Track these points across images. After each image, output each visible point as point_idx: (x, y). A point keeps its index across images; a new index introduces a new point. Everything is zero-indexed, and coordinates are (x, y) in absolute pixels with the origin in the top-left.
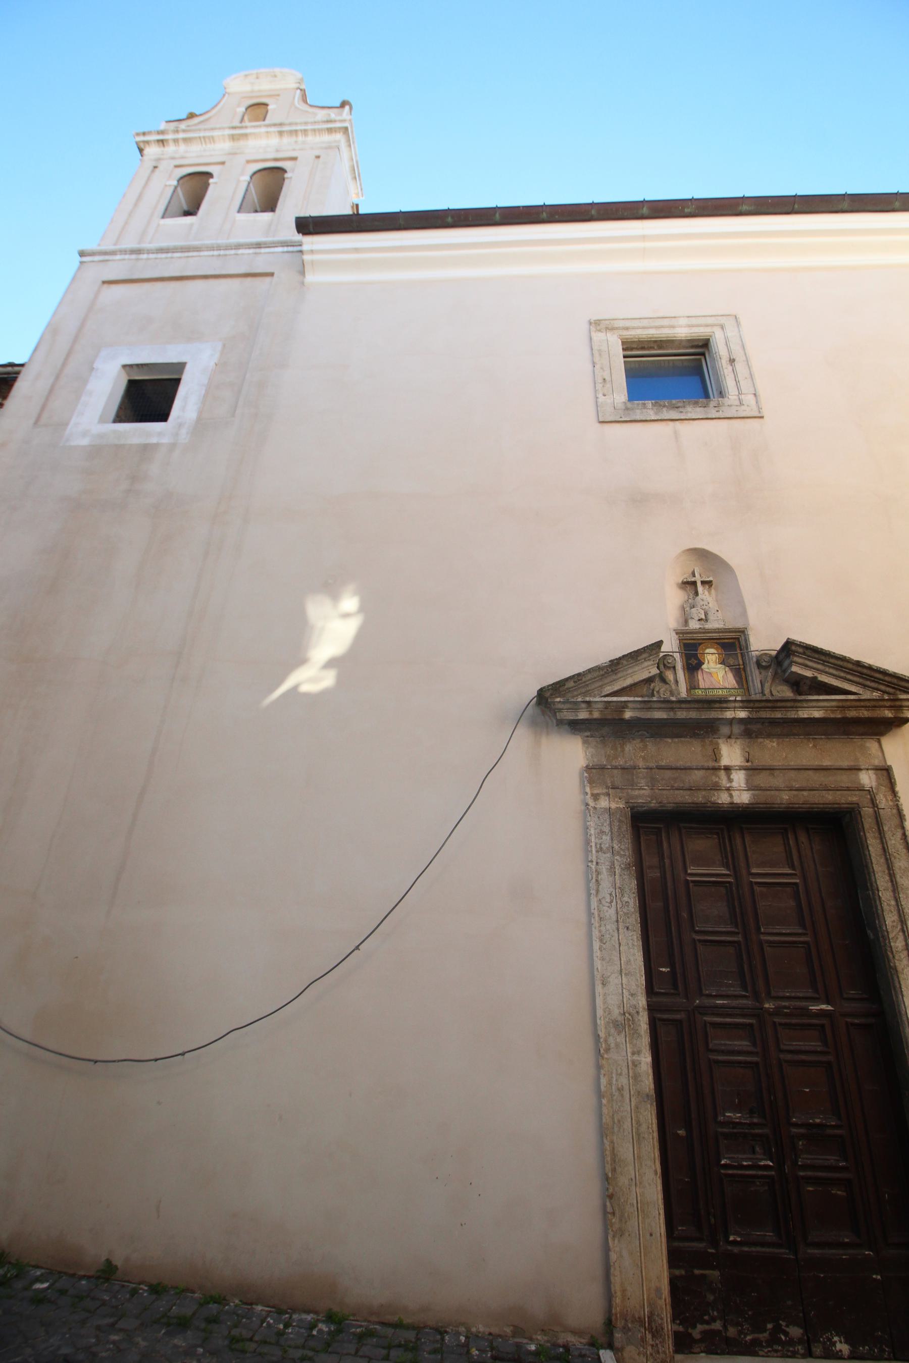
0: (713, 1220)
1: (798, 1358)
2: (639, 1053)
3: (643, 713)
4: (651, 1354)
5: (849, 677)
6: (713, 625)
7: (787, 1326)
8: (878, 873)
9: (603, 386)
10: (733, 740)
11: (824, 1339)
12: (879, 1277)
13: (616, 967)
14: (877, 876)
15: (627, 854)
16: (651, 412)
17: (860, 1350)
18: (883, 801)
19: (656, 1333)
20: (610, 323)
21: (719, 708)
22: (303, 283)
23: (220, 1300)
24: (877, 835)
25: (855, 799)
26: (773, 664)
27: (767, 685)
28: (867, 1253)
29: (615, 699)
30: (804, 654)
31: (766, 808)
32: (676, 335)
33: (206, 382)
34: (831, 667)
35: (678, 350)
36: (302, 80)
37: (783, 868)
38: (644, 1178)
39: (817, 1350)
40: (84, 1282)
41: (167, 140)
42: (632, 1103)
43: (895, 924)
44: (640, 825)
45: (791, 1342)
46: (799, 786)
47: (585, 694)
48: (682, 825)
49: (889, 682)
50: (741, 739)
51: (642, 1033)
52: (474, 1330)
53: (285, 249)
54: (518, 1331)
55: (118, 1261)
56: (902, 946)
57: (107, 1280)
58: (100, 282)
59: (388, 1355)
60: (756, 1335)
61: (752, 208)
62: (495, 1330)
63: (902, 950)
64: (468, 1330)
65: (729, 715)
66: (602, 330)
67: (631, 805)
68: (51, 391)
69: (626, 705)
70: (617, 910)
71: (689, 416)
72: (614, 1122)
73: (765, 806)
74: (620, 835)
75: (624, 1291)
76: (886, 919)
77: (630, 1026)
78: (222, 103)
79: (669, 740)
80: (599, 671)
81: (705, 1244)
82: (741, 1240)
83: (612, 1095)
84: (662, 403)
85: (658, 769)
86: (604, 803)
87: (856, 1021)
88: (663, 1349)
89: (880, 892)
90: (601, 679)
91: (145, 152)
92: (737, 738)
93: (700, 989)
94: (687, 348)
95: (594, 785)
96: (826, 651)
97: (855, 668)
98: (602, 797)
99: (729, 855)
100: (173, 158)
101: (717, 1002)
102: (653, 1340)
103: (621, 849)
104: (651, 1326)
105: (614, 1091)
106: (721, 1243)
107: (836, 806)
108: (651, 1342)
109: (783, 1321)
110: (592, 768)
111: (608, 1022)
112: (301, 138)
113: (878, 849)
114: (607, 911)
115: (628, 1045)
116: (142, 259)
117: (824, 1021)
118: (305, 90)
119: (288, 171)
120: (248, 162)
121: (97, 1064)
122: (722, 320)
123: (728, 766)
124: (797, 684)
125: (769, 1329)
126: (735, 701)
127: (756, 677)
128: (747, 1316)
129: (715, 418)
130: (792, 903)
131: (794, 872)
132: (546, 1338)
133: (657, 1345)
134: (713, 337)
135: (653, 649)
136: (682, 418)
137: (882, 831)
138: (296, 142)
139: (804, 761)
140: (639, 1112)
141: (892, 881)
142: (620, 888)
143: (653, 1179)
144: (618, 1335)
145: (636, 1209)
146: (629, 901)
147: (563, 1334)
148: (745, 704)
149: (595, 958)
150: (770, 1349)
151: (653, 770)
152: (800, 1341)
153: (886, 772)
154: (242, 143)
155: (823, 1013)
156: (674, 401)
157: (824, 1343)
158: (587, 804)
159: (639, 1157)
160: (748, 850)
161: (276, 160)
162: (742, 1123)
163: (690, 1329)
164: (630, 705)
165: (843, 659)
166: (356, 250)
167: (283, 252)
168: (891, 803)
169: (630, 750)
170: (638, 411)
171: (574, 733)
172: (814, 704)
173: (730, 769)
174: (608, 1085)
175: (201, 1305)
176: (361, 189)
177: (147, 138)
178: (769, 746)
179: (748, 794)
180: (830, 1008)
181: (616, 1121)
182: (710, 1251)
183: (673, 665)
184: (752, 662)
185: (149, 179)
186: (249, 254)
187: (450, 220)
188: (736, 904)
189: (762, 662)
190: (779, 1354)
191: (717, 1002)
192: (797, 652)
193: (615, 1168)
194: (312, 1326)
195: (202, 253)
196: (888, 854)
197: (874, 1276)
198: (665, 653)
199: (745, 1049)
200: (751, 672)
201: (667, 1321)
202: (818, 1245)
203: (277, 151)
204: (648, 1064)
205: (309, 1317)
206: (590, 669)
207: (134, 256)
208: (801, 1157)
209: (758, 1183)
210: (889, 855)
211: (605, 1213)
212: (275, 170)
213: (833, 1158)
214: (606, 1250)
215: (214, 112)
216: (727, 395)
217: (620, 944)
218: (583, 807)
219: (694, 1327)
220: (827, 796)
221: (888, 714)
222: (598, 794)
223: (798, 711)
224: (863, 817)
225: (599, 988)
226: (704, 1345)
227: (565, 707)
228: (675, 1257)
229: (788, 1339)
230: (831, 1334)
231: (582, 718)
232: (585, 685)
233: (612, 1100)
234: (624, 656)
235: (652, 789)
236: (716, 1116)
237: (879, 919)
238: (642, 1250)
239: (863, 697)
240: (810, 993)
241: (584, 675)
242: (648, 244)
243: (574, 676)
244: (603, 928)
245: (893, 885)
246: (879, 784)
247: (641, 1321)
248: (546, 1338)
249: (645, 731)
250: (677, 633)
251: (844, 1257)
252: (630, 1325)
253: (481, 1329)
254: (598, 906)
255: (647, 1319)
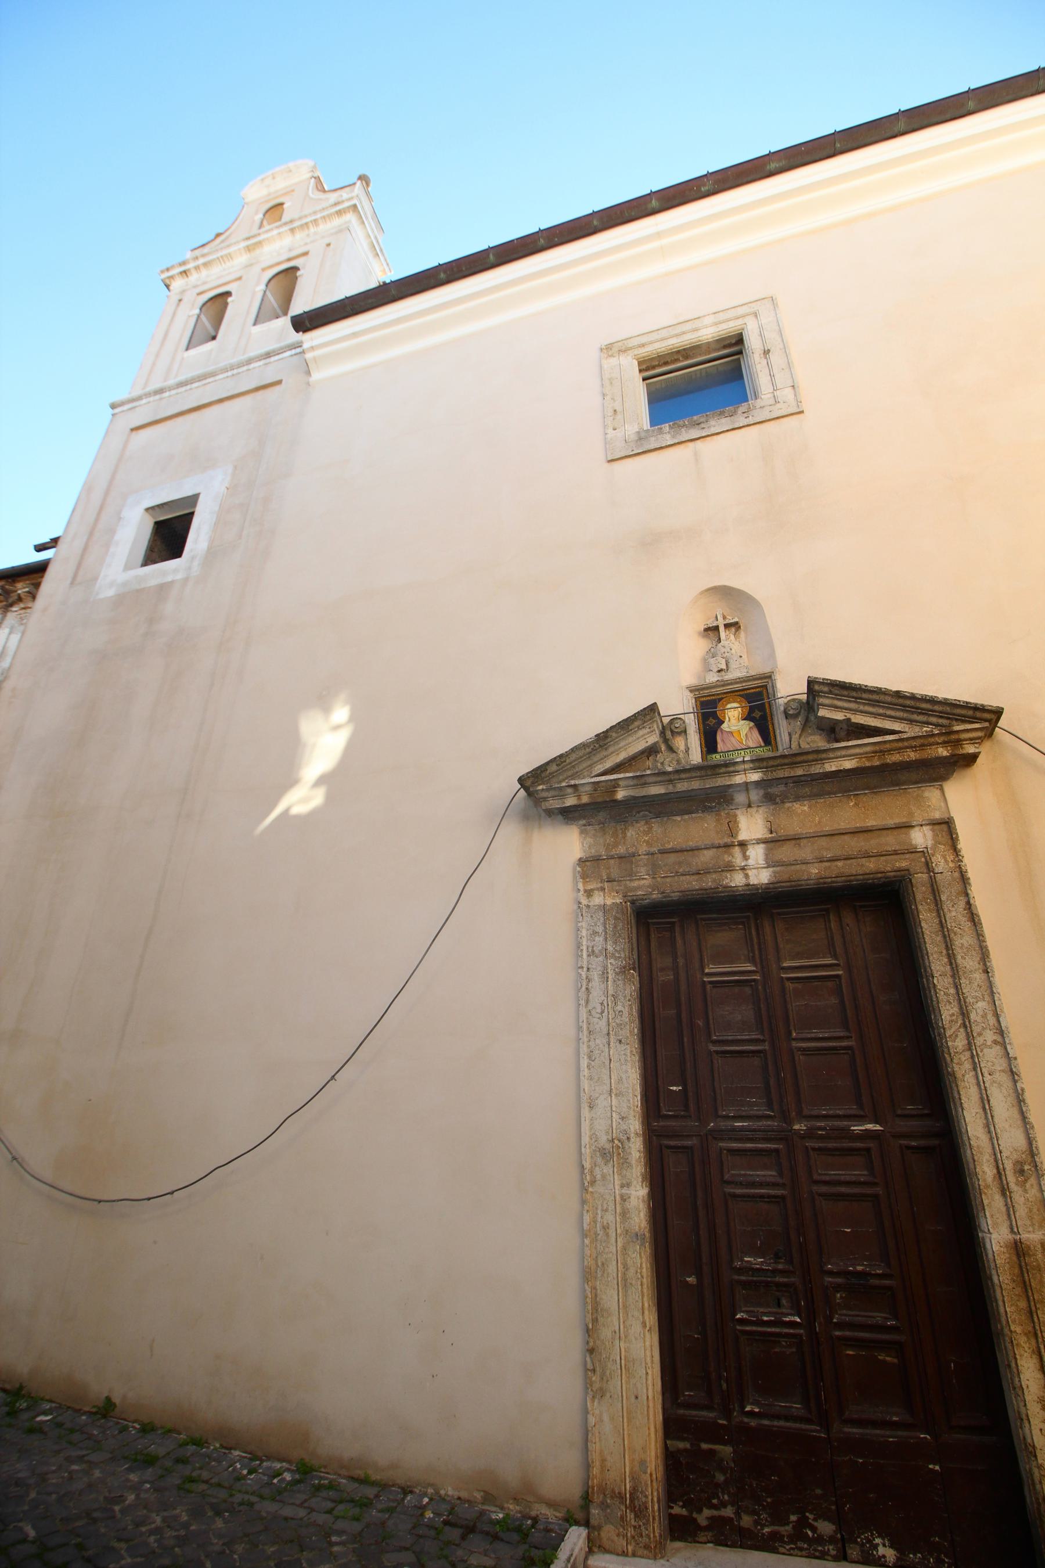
0: (724, 1386)
1: (827, 1560)
2: (628, 1185)
3: (637, 790)
4: (633, 1537)
5: (889, 712)
6: (734, 674)
7: (815, 1520)
8: (932, 955)
9: (614, 419)
10: (755, 809)
11: (862, 1539)
12: (937, 1468)
13: (605, 1087)
14: (931, 958)
15: (623, 955)
16: (668, 437)
17: (910, 1558)
18: (941, 863)
19: (640, 1512)
20: (624, 344)
21: (725, 773)
22: (308, 384)
23: (199, 1443)
24: (932, 906)
25: (904, 864)
26: (803, 711)
27: (795, 737)
28: (922, 1436)
29: (603, 778)
30: (830, 692)
31: (791, 886)
32: (700, 338)
33: (217, 508)
34: (864, 704)
35: (709, 354)
36: (315, 167)
37: (824, 957)
38: (629, 1331)
39: (854, 1552)
40: (84, 1418)
41: (189, 270)
42: (619, 1243)
43: (954, 1018)
44: (650, 921)
45: (820, 1540)
46: (832, 855)
47: (573, 777)
48: (699, 917)
49: (941, 712)
50: (764, 807)
51: (633, 1162)
52: (442, 1492)
53: (293, 352)
54: (489, 1498)
55: (116, 1400)
56: (963, 1046)
57: (104, 1416)
58: (129, 430)
59: (333, 1509)
60: (776, 1528)
61: (783, 163)
62: (464, 1495)
63: (963, 1051)
64: (437, 1493)
65: (739, 779)
66: (614, 355)
67: (629, 898)
68: (85, 549)
69: (618, 785)
70: (608, 1021)
71: (713, 430)
72: (597, 1266)
73: (788, 884)
74: (615, 934)
75: (603, 1461)
76: (942, 1012)
77: (619, 1154)
78: (239, 220)
79: (679, 818)
80: (585, 749)
81: (715, 1414)
82: (759, 1412)
83: (596, 1234)
84: (681, 423)
85: (661, 853)
86: (598, 899)
87: (914, 1144)
88: (647, 1532)
89: (935, 979)
90: (589, 757)
91: (171, 288)
92: (758, 806)
93: (716, 1110)
94: (718, 350)
95: (588, 880)
96: (855, 685)
97: (894, 700)
98: (596, 892)
99: (756, 947)
100: (196, 286)
101: (736, 1124)
102: (635, 1521)
103: (616, 950)
104: (634, 1504)
105: (598, 1229)
106: (735, 1414)
107: (880, 875)
108: (633, 1522)
109: (811, 1513)
110: (585, 861)
111: (594, 1151)
112: (312, 229)
113: (934, 925)
114: (597, 1023)
115: (616, 1177)
116: (164, 398)
117: (871, 1144)
118: (319, 177)
119: (300, 268)
120: (263, 270)
121: (101, 1203)
122: (755, 307)
123: (743, 840)
124: (832, 730)
125: (794, 1522)
126: (744, 762)
127: (784, 731)
128: (765, 1503)
129: (743, 427)
130: (834, 1000)
131: (836, 962)
132: (518, 1508)
133: (640, 1526)
134: (746, 330)
135: (646, 714)
136: (703, 435)
137: (939, 902)
138: (308, 235)
139: (842, 824)
140: (626, 1254)
141: (951, 964)
142: (613, 995)
143: (641, 1332)
144: (595, 1511)
145: (619, 1367)
146: (623, 1009)
147: (537, 1505)
148: (757, 764)
149: (582, 1078)
150: (793, 1546)
151: (656, 856)
152: (832, 1540)
153: (946, 827)
154: (258, 252)
155: (868, 1135)
156: (695, 418)
157: (863, 1545)
158: (580, 903)
159: (625, 1307)
160: (779, 939)
161: (289, 260)
162: (763, 1270)
163: (694, 1513)
164: (621, 783)
165: (878, 691)
166: (355, 335)
167: (292, 356)
168: (951, 865)
169: (632, 835)
170: (653, 439)
171: (567, 824)
172: (843, 753)
173: (746, 845)
174: (592, 1223)
175: (181, 1446)
176: (388, 264)
177: (171, 273)
178: (799, 811)
179: (767, 871)
180: (878, 1127)
181: (600, 1264)
182: (720, 1422)
183: (683, 729)
184: (779, 712)
185: (174, 314)
186: (260, 366)
187: (442, 276)
188: (762, 1006)
189: (789, 710)
190: (804, 1553)
191: (736, 1124)
192: (822, 692)
193: (597, 1319)
194: (278, 1474)
195: (217, 378)
196: (946, 930)
197: (931, 1466)
198: (672, 717)
199: (772, 1180)
200: (779, 724)
201: (652, 1499)
202: (860, 1423)
203: (290, 250)
204: (639, 1199)
205: (278, 1465)
206: (574, 748)
207: (157, 397)
208: (839, 1312)
209: (784, 1343)
210: (948, 931)
211: (586, 1370)
212: (290, 271)
213: (882, 1315)
214: (586, 1412)
215: (233, 228)
216: (760, 395)
217: (610, 1060)
218: (576, 907)
219: (700, 1511)
220: (867, 864)
221: (942, 752)
222: (592, 890)
223: (823, 763)
224: (914, 885)
225: (585, 1112)
226: (710, 1534)
227: (549, 796)
228: (672, 1426)
229: (816, 1535)
230: (872, 1535)
231: (569, 805)
232: (571, 767)
233: (597, 1240)
234: (612, 728)
235: (653, 878)
236: (731, 1261)
237: (934, 1013)
238: (625, 1414)
239: (905, 736)
240: (854, 1110)
241: (567, 756)
242: (665, 241)
243: (555, 758)
244: (592, 1043)
245: (952, 968)
246: (937, 843)
247: (621, 1497)
248: (518, 1508)
249: (646, 811)
250: (691, 691)
251: (891, 1439)
252: (609, 1501)
253: (450, 1493)
254: (587, 1018)
255: (628, 1496)
